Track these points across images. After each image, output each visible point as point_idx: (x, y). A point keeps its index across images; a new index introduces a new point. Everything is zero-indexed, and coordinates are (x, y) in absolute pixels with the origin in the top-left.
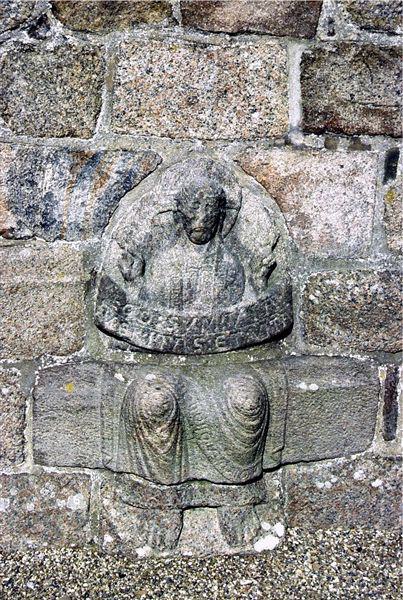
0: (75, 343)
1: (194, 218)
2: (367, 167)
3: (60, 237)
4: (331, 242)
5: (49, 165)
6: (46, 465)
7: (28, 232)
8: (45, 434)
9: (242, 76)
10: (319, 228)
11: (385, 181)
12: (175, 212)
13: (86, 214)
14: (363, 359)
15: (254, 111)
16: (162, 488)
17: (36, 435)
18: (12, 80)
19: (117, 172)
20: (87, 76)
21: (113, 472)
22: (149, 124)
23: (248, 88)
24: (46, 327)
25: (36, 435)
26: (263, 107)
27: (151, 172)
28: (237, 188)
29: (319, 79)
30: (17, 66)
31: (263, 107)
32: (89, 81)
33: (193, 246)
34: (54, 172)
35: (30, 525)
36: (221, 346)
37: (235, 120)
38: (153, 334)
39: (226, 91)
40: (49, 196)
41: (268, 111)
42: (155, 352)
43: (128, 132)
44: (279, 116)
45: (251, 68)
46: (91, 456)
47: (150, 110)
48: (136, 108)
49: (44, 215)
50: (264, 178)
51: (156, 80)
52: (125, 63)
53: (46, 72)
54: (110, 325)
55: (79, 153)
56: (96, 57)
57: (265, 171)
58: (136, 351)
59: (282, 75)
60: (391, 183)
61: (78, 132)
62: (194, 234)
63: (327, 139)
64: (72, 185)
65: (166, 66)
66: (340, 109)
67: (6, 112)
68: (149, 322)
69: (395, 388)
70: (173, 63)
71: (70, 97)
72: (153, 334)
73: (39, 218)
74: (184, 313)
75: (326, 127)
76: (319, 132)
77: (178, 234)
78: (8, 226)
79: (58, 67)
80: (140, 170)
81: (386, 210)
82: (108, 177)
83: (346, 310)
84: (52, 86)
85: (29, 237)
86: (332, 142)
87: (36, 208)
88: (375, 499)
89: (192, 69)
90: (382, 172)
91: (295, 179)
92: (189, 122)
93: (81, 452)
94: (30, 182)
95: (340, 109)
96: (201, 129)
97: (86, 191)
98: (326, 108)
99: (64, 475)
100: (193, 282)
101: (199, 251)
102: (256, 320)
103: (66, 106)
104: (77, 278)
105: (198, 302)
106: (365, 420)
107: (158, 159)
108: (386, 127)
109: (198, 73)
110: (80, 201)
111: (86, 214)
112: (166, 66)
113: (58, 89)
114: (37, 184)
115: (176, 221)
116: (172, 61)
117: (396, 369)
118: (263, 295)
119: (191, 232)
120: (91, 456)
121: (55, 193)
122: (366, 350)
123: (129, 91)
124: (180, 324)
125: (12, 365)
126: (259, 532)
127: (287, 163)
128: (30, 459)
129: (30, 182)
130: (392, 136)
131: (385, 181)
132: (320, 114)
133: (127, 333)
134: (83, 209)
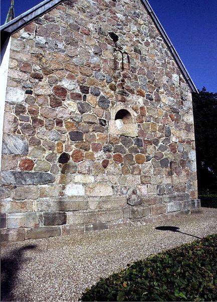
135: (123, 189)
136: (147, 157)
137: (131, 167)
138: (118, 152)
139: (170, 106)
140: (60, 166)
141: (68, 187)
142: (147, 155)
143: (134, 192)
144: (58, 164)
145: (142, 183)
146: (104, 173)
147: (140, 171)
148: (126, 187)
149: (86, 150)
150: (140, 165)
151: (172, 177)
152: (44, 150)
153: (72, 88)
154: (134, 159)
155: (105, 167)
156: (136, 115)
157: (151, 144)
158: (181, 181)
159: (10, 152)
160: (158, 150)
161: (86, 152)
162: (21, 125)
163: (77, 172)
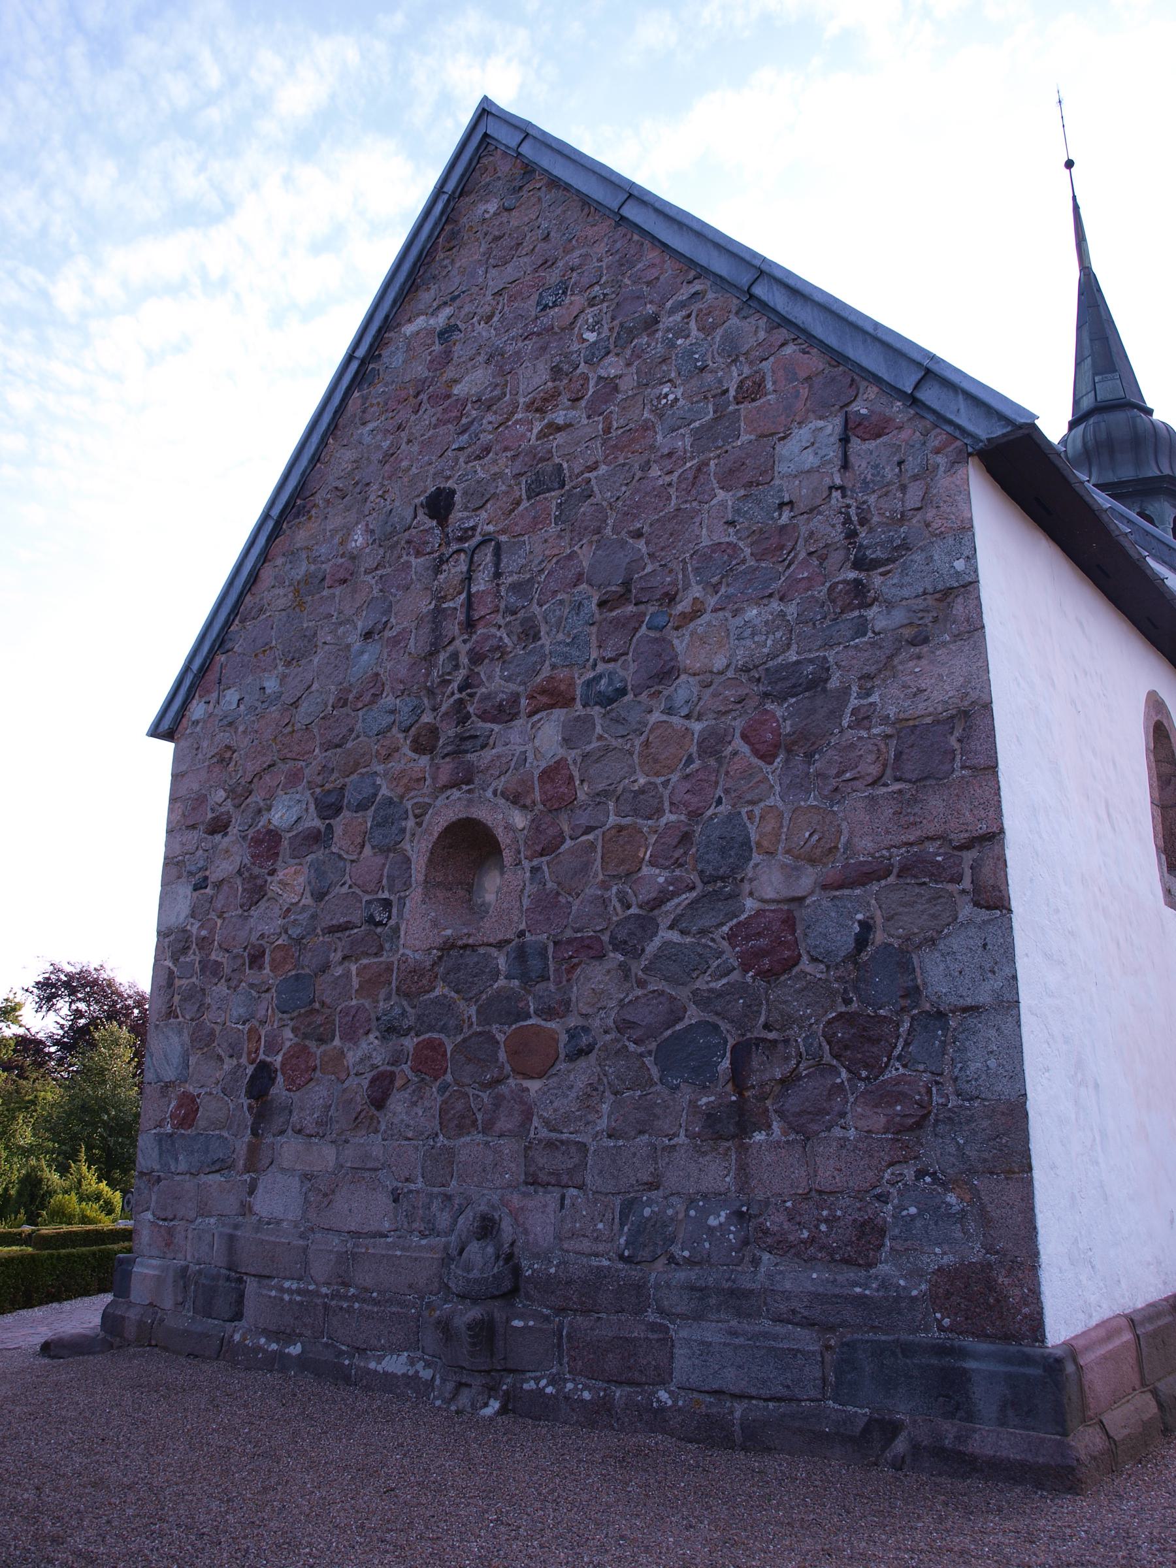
7: (427, 1233)
55: (445, 1195)
66: (538, 1172)
76: (532, 1184)
91: (522, 1208)
126: (486, 1405)
135: (434, 1207)
136: (573, 1034)
137: (484, 1096)
138: (431, 1028)
139: (746, 669)
140: (250, 1108)
141: (264, 1182)
142: (573, 1021)
143: (487, 1228)
144: (246, 1102)
145: (533, 1181)
146: (376, 1131)
147: (528, 1116)
148: (448, 1198)
149: (321, 1040)
150: (534, 1086)
151: (743, 1149)
152: (220, 1058)
153: (295, 818)
154: (502, 1056)
155: (379, 1103)
156: (520, 820)
157: (601, 957)
158: (827, 1175)
159: (158, 1077)
160: (641, 984)
161: (323, 1048)
162: (347, 975)
163: (290, 1131)
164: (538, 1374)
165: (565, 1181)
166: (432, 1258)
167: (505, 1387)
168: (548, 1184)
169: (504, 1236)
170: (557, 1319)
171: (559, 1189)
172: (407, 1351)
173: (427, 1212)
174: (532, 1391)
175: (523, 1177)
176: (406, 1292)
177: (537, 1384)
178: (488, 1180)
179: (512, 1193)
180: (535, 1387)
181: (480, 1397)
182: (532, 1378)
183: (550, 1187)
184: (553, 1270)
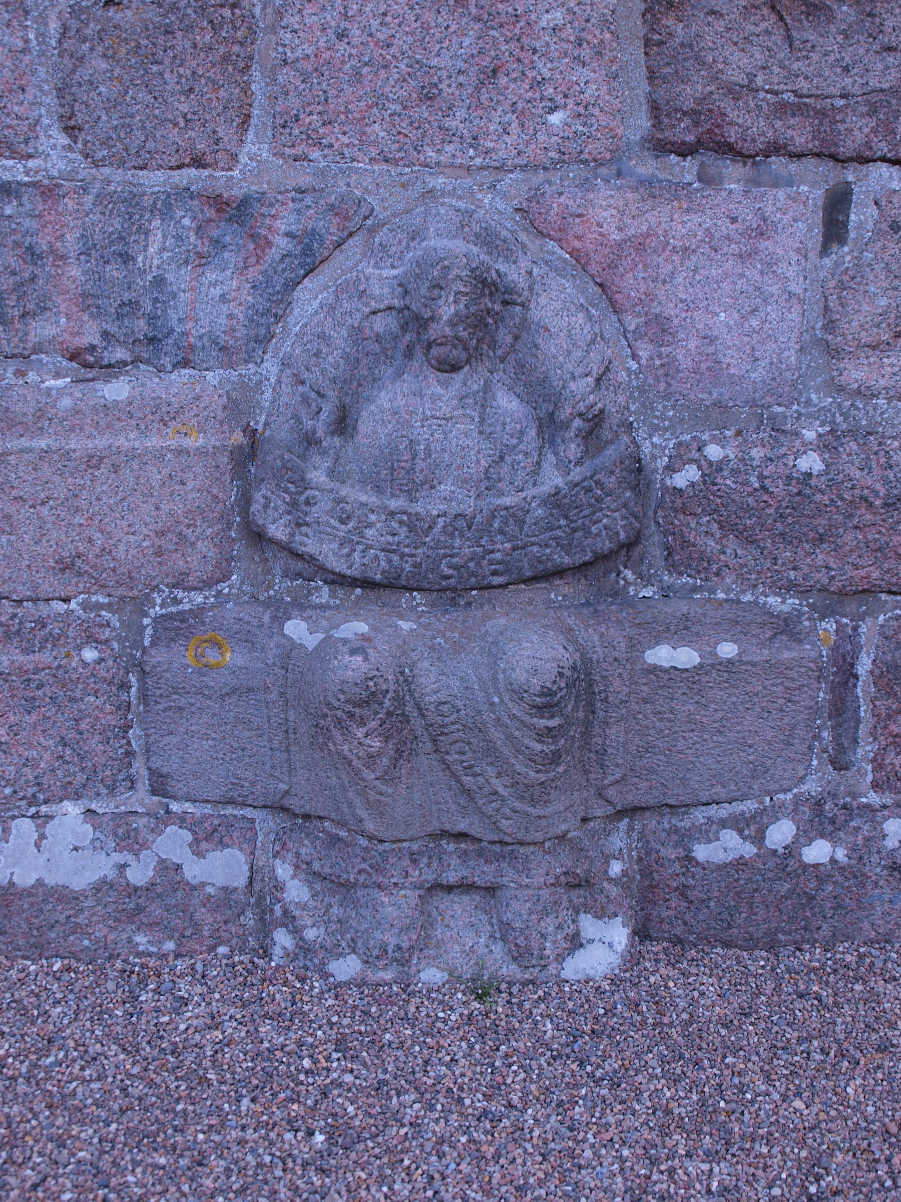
0: (218, 566)
1: (432, 318)
2: (786, 219)
3: (186, 363)
4: (716, 368)
5: (157, 223)
6: (174, 798)
7: (121, 354)
8: (167, 740)
9: (525, 40)
10: (692, 345)
11: (824, 251)
12: (400, 311)
13: (231, 317)
14: (785, 608)
15: (552, 111)
16: (381, 847)
17: (151, 739)
18: (81, 59)
19: (286, 235)
20: (222, 50)
21: (296, 816)
22: (345, 140)
23: (540, 65)
24: (160, 534)
25: (151, 739)
26: (571, 102)
27: (351, 235)
28: (524, 263)
29: (682, 45)
30: (88, 32)
31: (571, 102)
32: (226, 59)
33: (433, 376)
34: (165, 237)
35: (139, 909)
36: (495, 573)
37: (514, 129)
38: (360, 548)
39: (494, 71)
40: (159, 282)
41: (581, 110)
42: (367, 584)
43: (306, 158)
44: (604, 120)
45: (543, 23)
46: (253, 784)
47: (347, 112)
48: (320, 108)
49: (152, 318)
50: (577, 244)
51: (354, 51)
52: (293, 20)
53: (144, 42)
54: (278, 531)
55: (218, 202)
56: (237, 11)
57: (578, 230)
58: (333, 582)
59: (607, 36)
60: (845, 253)
61: (209, 159)
62: (434, 351)
63: (702, 165)
64: (202, 260)
65: (375, 23)
66: (727, 105)
67: (73, 123)
68: (351, 525)
69: (852, 665)
70: (388, 19)
71: (191, 90)
72: (360, 548)
73: (141, 325)
74: (418, 508)
75: (699, 142)
76: (684, 151)
77: (409, 353)
78: (84, 341)
79: (167, 32)
80: (331, 229)
81: (826, 308)
82: (270, 244)
83: (749, 508)
84: (155, 68)
85: (125, 364)
86: (711, 171)
87: (133, 305)
88: (813, 884)
89: (426, 28)
90: (818, 231)
91: (640, 245)
92: (424, 135)
93: (234, 775)
94: (121, 255)
95: (727, 105)
96: (449, 148)
97: (228, 273)
98: (699, 101)
99: (205, 817)
100: (436, 447)
101: (445, 385)
102: (563, 522)
103: (184, 108)
104: (214, 441)
105: (445, 488)
106: (794, 727)
107: (364, 210)
108: (823, 140)
109: (438, 36)
110: (216, 292)
111: (231, 317)
112: (375, 23)
113: (167, 76)
114: (134, 259)
115: (404, 328)
116: (385, 14)
117: (855, 629)
118: (577, 474)
119: (429, 346)
120: (253, 784)
121: (170, 277)
122: (791, 588)
123: (306, 79)
124: (411, 529)
125: (99, 606)
126: (576, 943)
127: (622, 213)
128: (143, 786)
129: (121, 255)
130: (834, 157)
131: (824, 251)
132: (685, 114)
133: (310, 546)
134: (224, 308)
164: (750, 806)
165: (859, 137)
166: (180, 452)
167: (616, 868)
168: (775, 149)
169: (551, 347)
170: (830, 625)
171: (825, 167)
172: (77, 796)
173: (113, 271)
174: (740, 863)
175: (642, 122)
176: (45, 589)
177: (759, 839)
178: (449, 136)
179: (585, 185)
180: (749, 850)
181: (549, 924)
182: (724, 824)
183: (777, 163)
184: (811, 462)
